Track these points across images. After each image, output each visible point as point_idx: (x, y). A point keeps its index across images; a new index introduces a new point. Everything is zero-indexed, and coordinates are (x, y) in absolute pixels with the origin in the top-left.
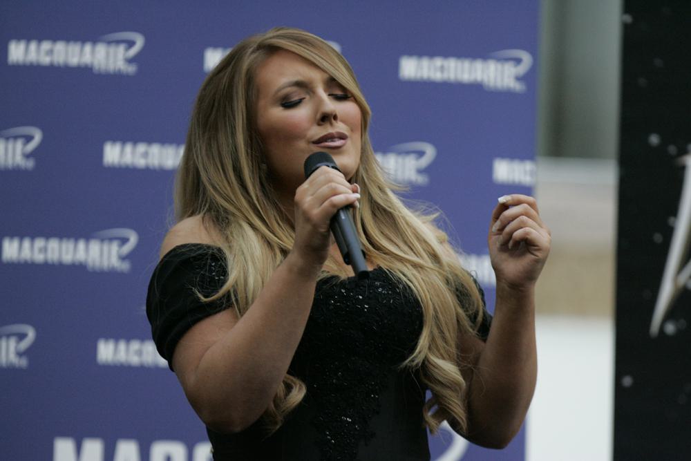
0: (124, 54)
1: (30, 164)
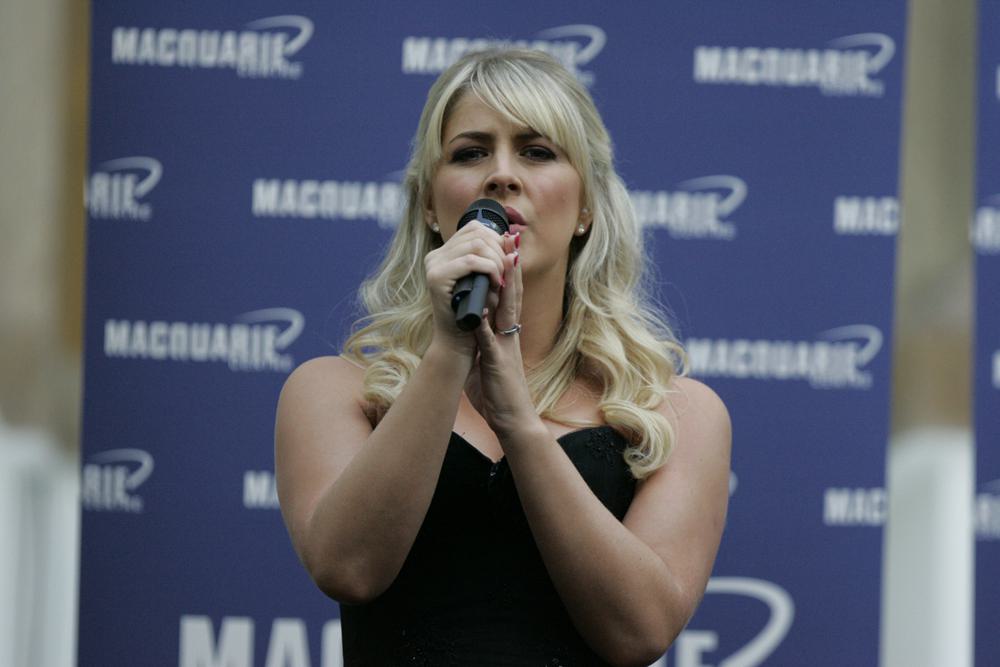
0: (283, 49)
1: (136, 504)
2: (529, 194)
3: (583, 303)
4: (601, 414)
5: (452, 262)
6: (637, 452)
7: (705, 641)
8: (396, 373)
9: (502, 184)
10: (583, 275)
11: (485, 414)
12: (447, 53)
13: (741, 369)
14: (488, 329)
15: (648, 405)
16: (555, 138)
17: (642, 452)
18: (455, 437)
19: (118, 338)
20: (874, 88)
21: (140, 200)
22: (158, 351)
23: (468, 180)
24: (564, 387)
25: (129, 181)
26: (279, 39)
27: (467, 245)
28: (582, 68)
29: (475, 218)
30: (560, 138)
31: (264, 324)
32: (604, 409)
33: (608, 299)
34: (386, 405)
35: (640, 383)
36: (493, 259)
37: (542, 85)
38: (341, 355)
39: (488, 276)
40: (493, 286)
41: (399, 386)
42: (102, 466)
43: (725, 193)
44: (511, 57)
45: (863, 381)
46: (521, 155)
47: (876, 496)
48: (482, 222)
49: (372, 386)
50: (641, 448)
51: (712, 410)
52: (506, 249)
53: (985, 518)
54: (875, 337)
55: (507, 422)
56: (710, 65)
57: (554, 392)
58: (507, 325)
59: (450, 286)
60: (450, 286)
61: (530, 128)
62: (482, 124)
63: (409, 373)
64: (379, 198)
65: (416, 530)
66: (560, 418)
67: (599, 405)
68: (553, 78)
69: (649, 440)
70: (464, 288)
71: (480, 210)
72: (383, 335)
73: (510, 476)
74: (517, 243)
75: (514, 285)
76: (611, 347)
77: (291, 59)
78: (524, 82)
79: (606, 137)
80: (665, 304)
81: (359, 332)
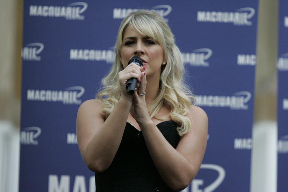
0: (79, 12)
2: (147, 54)
3: (165, 85)
4: (170, 117)
5: (126, 75)
6: (181, 128)
7: (200, 182)
8: (111, 105)
9: (139, 52)
10: (164, 77)
11: (135, 118)
12: (126, 13)
13: (210, 104)
14: (136, 94)
15: (184, 115)
16: (154, 38)
17: (182, 128)
18: (128, 124)
19: (31, 95)
20: (249, 23)
21: (38, 55)
22: (43, 99)
23: (129, 51)
24: (160, 109)
25: (34, 50)
26: (78, 9)
27: (130, 70)
28: (165, 17)
29: (133, 62)
30: (156, 38)
31: (73, 91)
32: (171, 116)
33: (172, 83)
34: (108, 114)
35: (182, 108)
36: (138, 74)
37: (151, 23)
38: (96, 99)
39: (136, 79)
40: (138, 81)
41: (112, 108)
42: (26, 132)
43: (206, 53)
44: (142, 14)
45: (245, 107)
46: (145, 43)
47: (249, 141)
48: (134, 63)
49: (104, 108)
50: (182, 127)
51: (203, 115)
52: (142, 71)
53: (280, 147)
54: (249, 95)
55: (142, 120)
56: (202, 16)
57: (157, 110)
58: (142, 93)
59: (125, 81)
60: (125, 81)
61: (147, 36)
62: (133, 35)
63: (115, 105)
64: (106, 55)
65: (116, 151)
66: (158, 118)
67: (170, 115)
68: (155, 20)
69: (184, 125)
70: (130, 82)
71: (134, 59)
72: (108, 92)
73: (143, 136)
74: (144, 69)
75: (144, 81)
76: (173, 97)
77: (81, 14)
78: (145, 22)
79: (172, 35)
80: (191, 85)
81: (101, 92)
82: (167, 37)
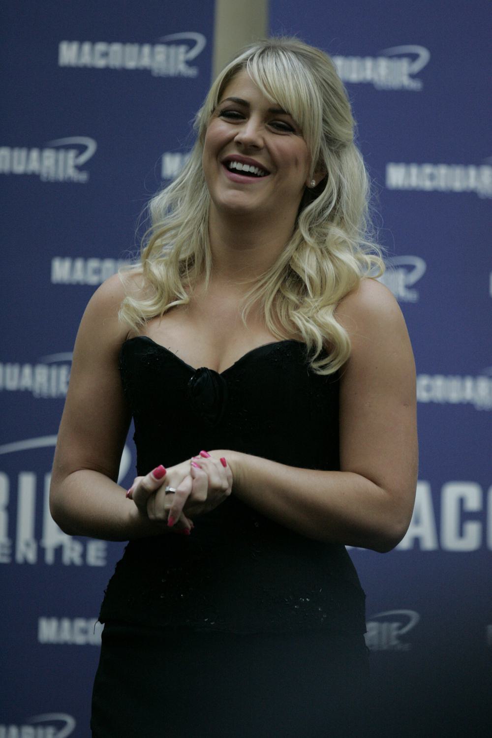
26: (72, 154)
77: (79, 168)
82: (331, 120)
